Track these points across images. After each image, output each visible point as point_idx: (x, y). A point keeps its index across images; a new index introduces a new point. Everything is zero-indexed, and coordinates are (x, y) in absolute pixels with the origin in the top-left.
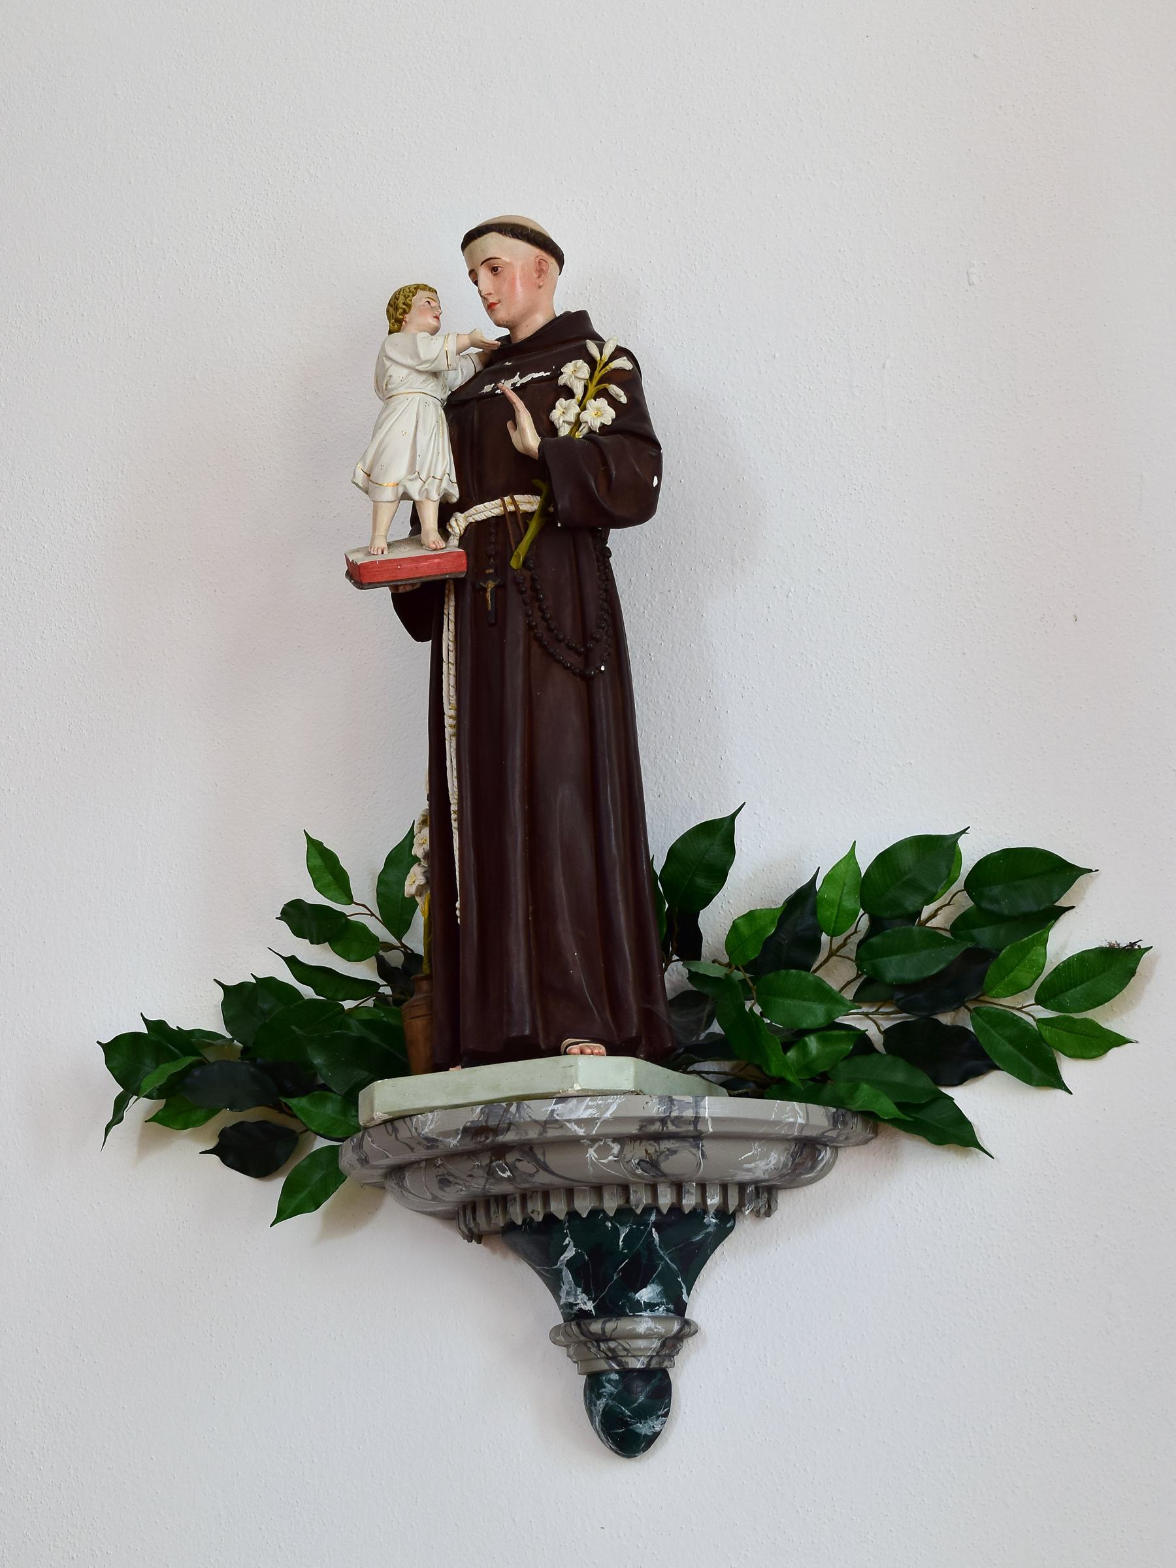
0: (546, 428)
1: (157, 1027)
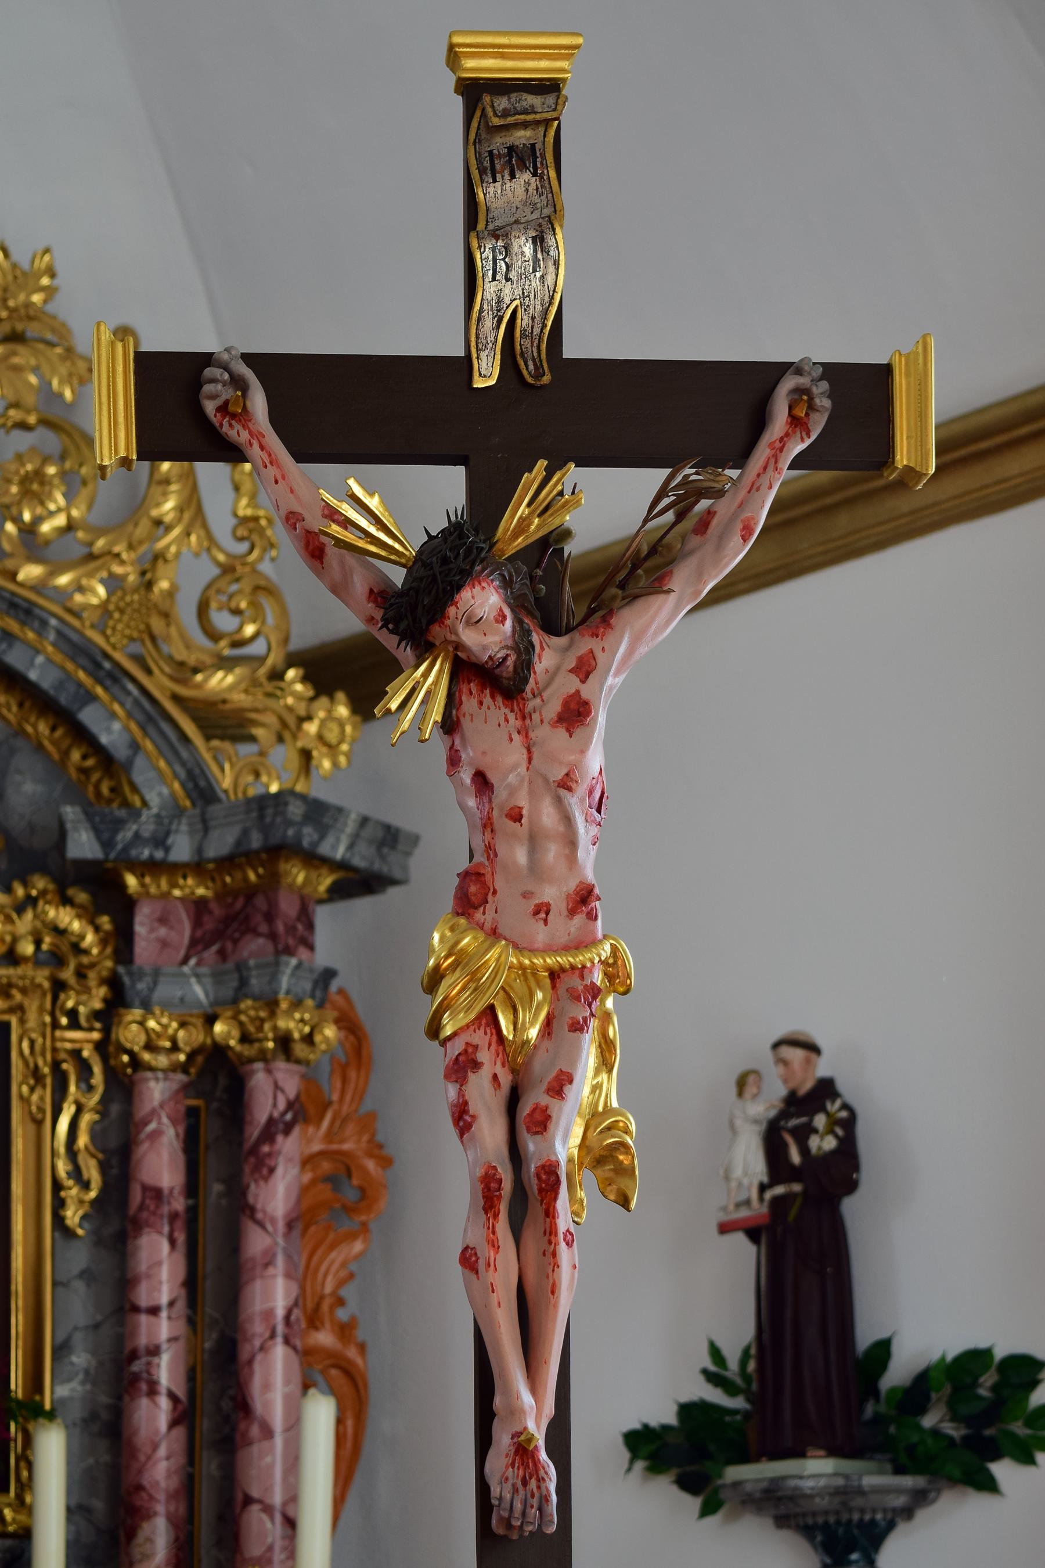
0: (804, 1150)
1: (646, 1427)
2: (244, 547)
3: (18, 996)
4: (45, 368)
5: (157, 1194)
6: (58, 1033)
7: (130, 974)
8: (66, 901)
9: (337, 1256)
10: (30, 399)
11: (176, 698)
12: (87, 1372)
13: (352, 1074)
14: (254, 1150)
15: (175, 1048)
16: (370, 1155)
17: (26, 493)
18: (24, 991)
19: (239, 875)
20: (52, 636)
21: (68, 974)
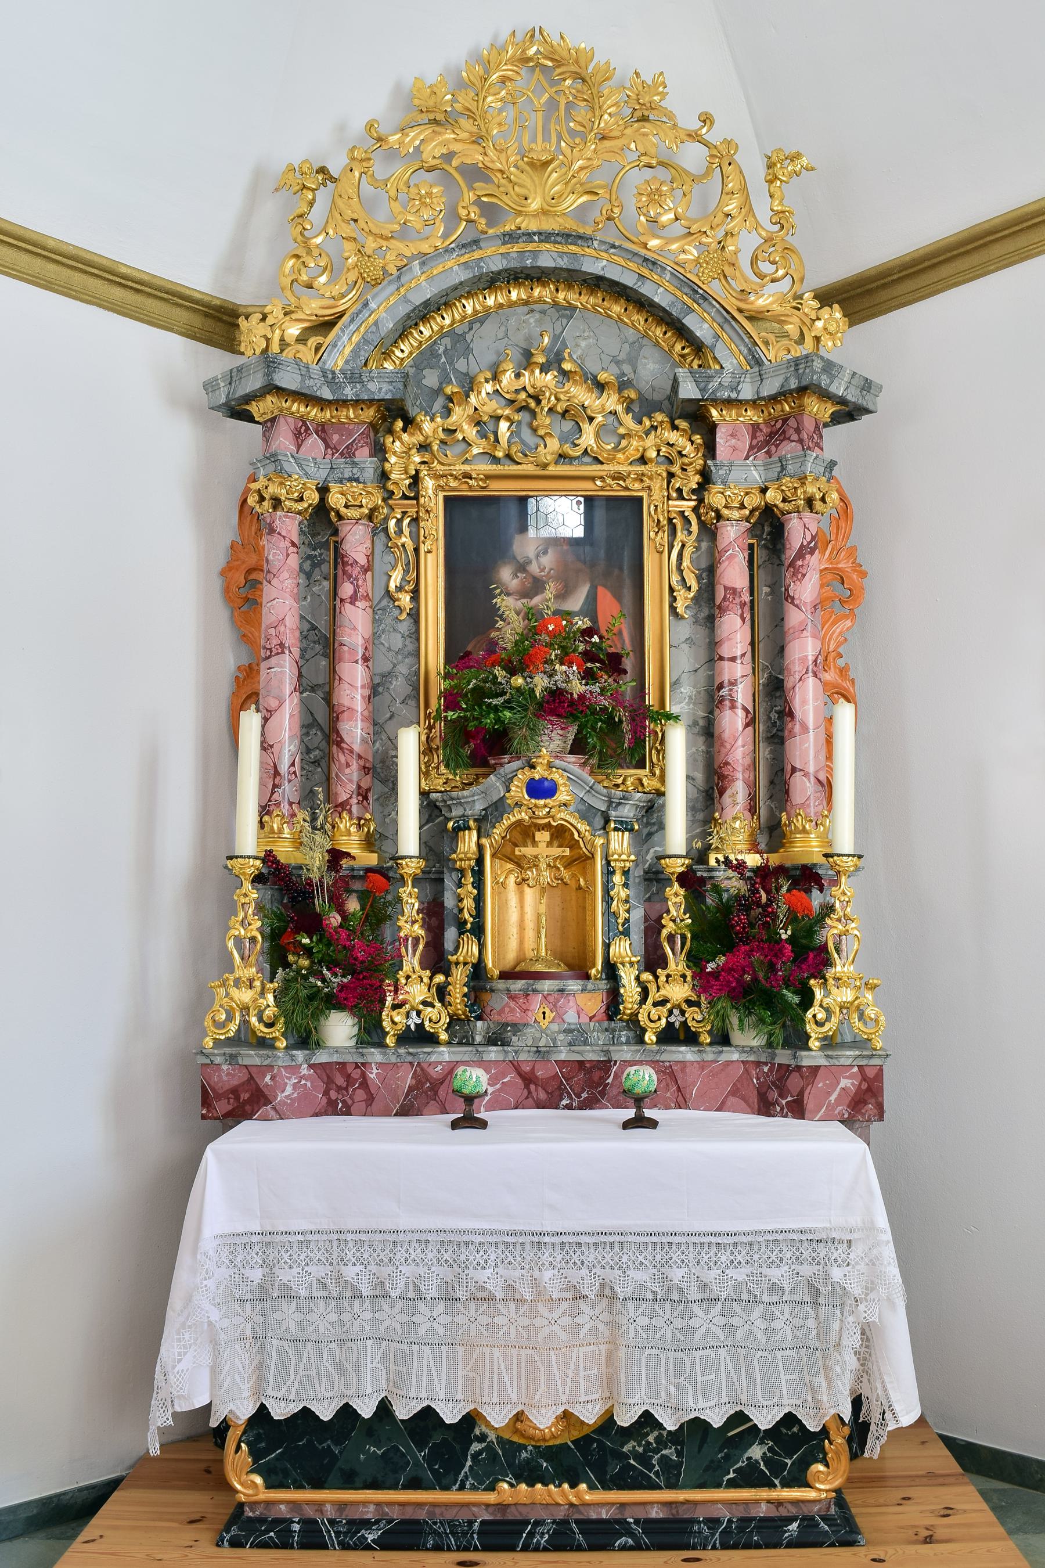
2: (777, 227)
3: (647, 482)
4: (662, 135)
5: (734, 591)
6: (670, 502)
7: (715, 466)
8: (675, 427)
9: (838, 628)
10: (652, 151)
11: (740, 311)
12: (690, 697)
13: (842, 524)
14: (792, 564)
15: (742, 506)
16: (855, 571)
17: (651, 201)
18: (651, 478)
19: (778, 407)
20: (668, 276)
21: (676, 469)
